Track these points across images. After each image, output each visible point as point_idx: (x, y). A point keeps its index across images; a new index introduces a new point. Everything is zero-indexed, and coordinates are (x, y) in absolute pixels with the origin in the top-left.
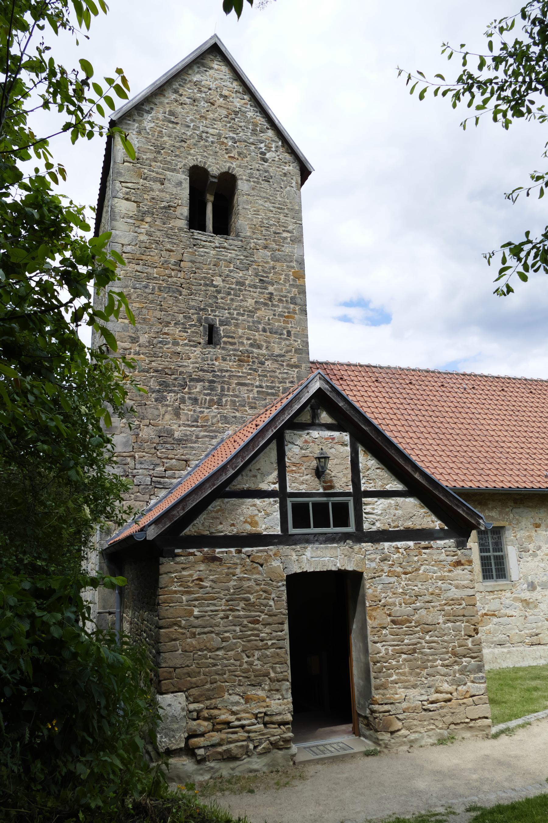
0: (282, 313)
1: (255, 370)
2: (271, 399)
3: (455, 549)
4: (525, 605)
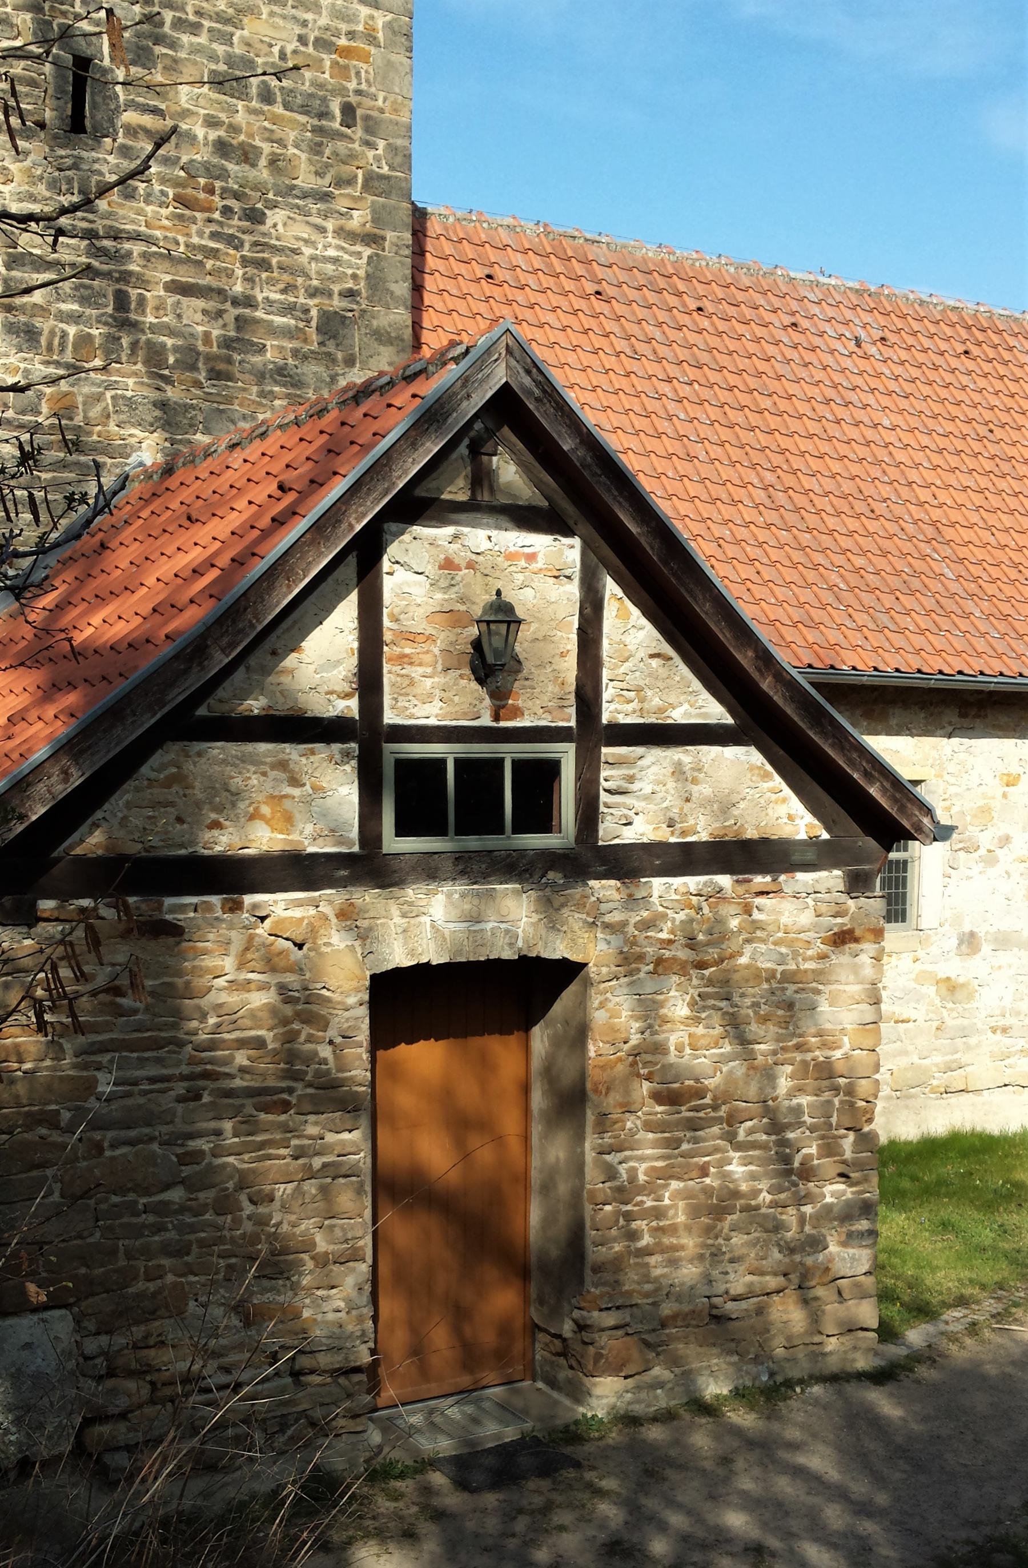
0: (327, 36)
1: (232, 241)
2: (281, 349)
3: (844, 897)
4: (944, 991)
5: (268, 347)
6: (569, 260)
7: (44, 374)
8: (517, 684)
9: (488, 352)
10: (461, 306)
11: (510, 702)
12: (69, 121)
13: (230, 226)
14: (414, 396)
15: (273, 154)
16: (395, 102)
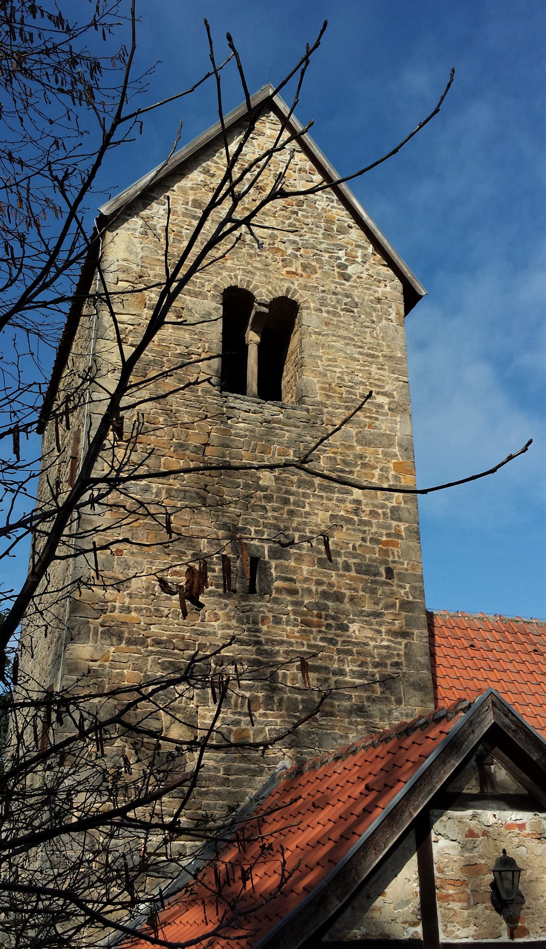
0: (376, 537)
5: (353, 697)
6: (516, 633)
7: (232, 720)
8: (522, 912)
9: (482, 705)
10: (457, 663)
11: (520, 924)
12: (248, 588)
13: (330, 634)
14: (441, 732)
15: (352, 595)
16: (413, 565)
